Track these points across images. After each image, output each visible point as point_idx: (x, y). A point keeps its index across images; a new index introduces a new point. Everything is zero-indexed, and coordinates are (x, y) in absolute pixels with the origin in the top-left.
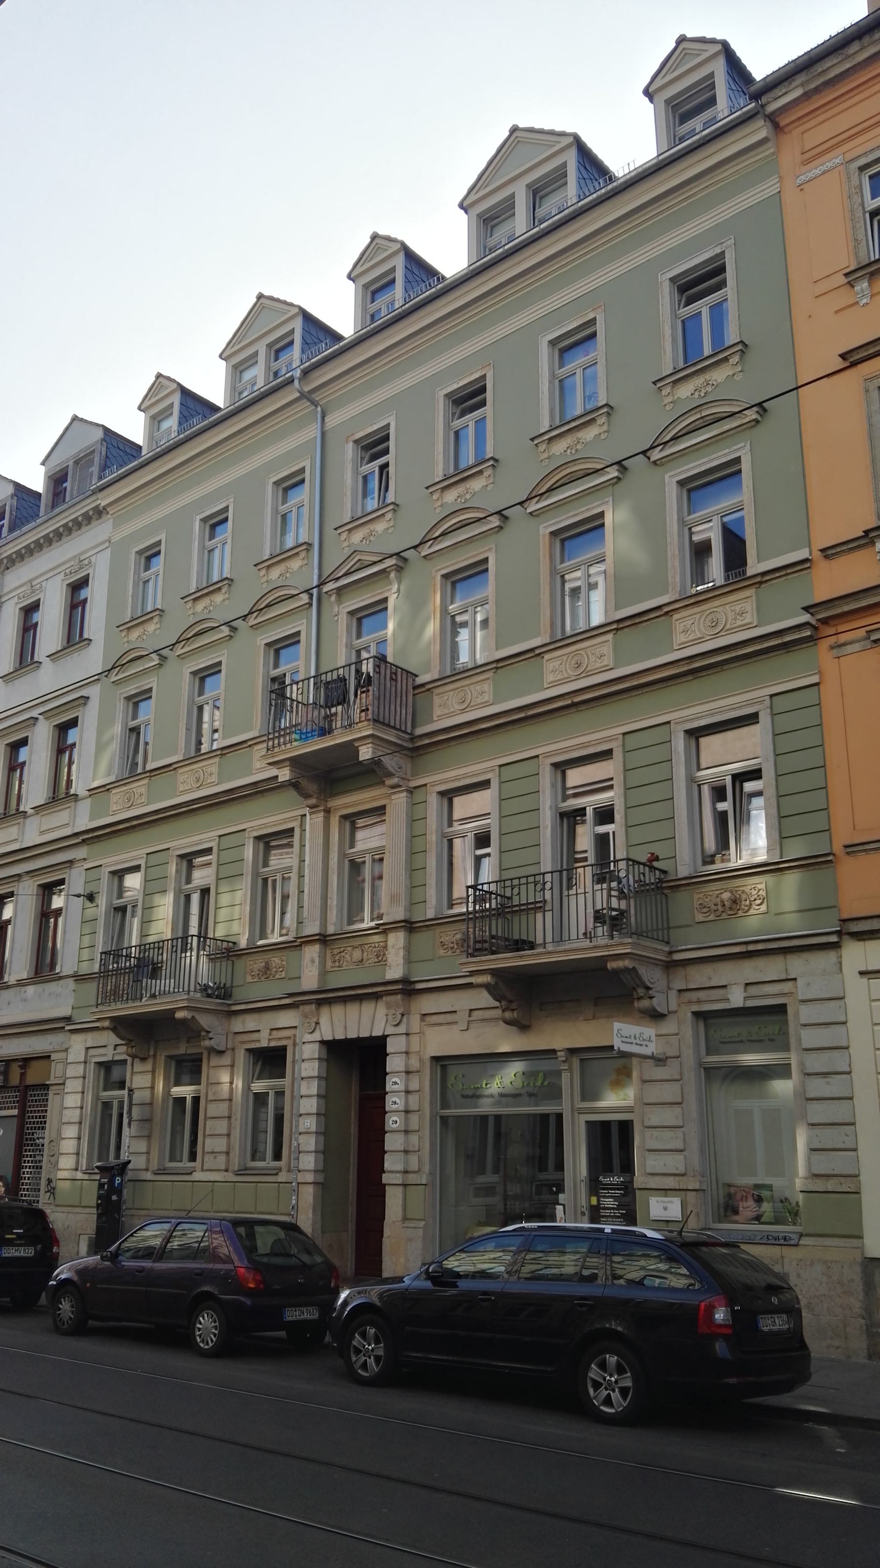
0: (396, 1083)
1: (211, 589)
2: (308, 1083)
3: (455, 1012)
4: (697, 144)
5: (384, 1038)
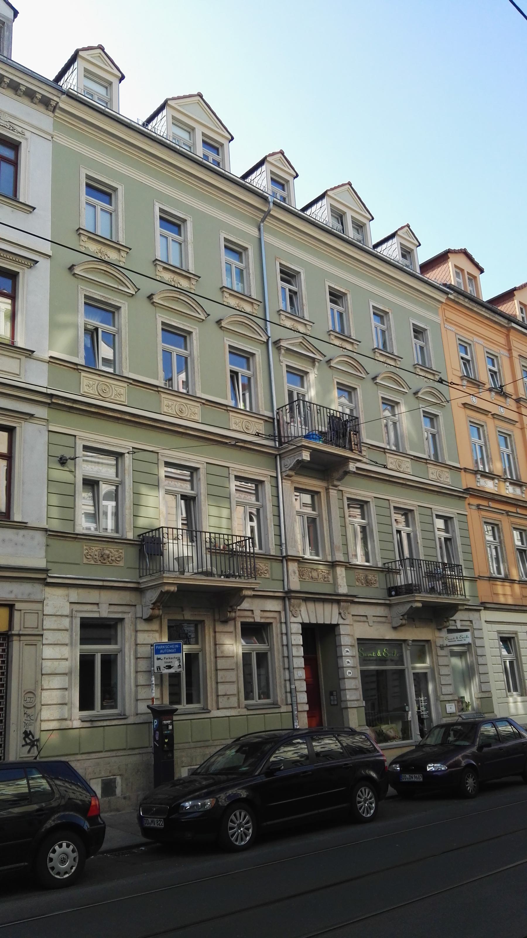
0: (348, 651)
1: (390, 356)
2: (297, 648)
3: (261, 611)
4: (126, 124)
5: (338, 625)
